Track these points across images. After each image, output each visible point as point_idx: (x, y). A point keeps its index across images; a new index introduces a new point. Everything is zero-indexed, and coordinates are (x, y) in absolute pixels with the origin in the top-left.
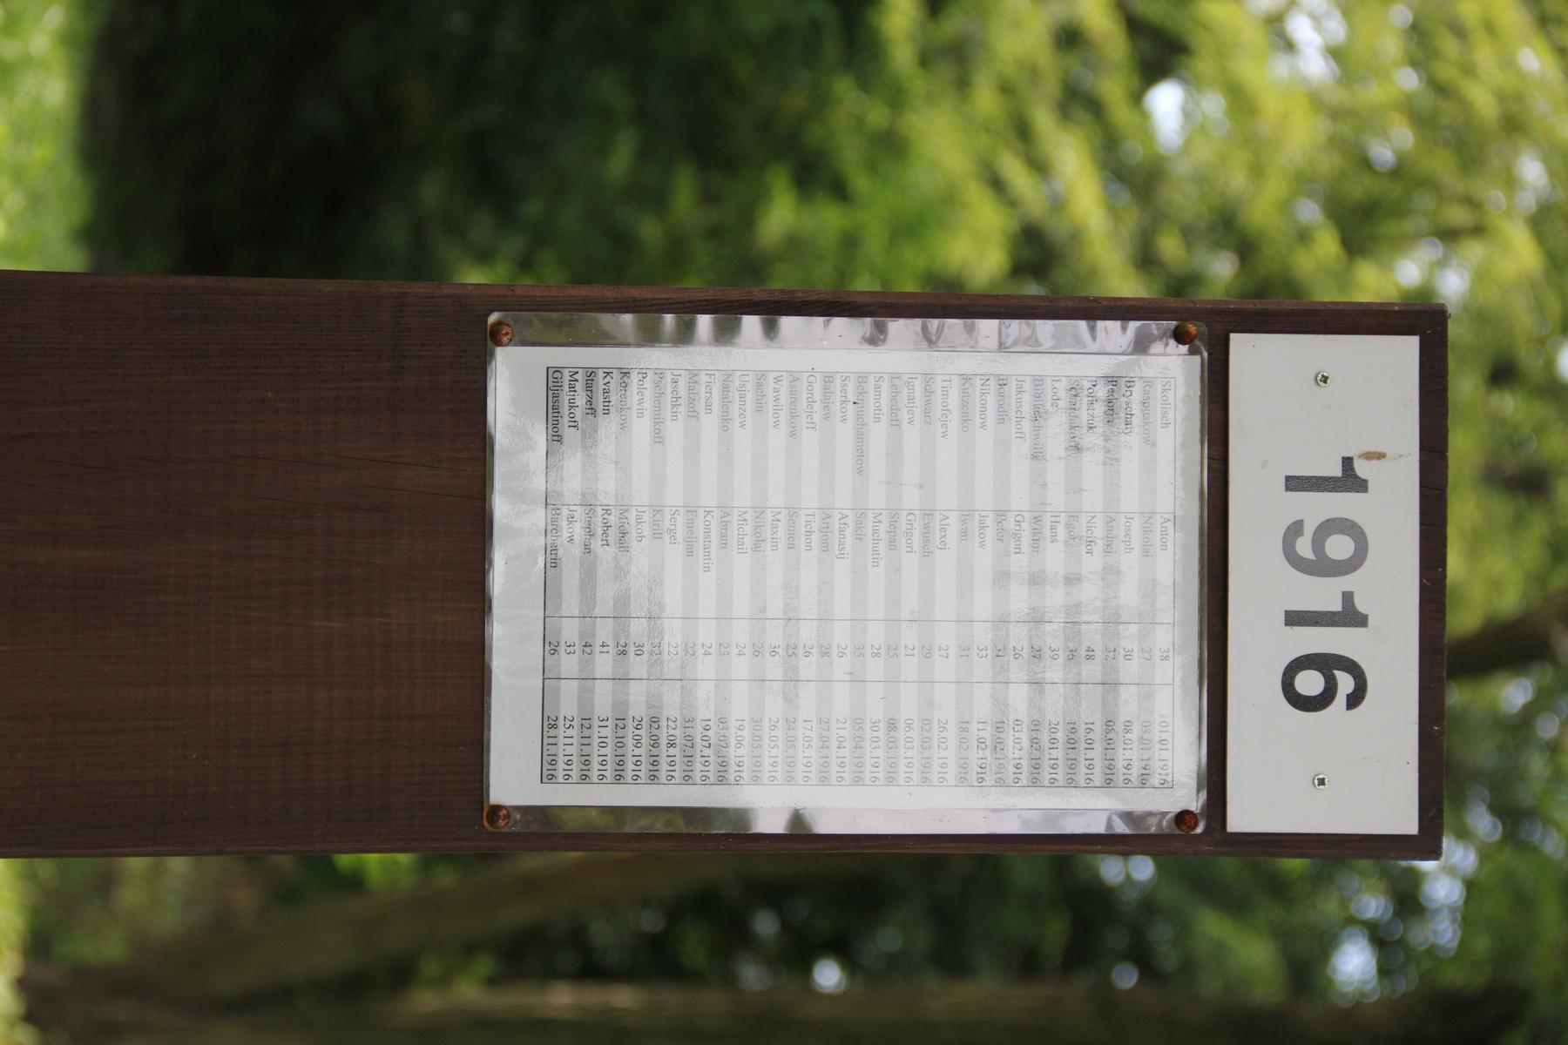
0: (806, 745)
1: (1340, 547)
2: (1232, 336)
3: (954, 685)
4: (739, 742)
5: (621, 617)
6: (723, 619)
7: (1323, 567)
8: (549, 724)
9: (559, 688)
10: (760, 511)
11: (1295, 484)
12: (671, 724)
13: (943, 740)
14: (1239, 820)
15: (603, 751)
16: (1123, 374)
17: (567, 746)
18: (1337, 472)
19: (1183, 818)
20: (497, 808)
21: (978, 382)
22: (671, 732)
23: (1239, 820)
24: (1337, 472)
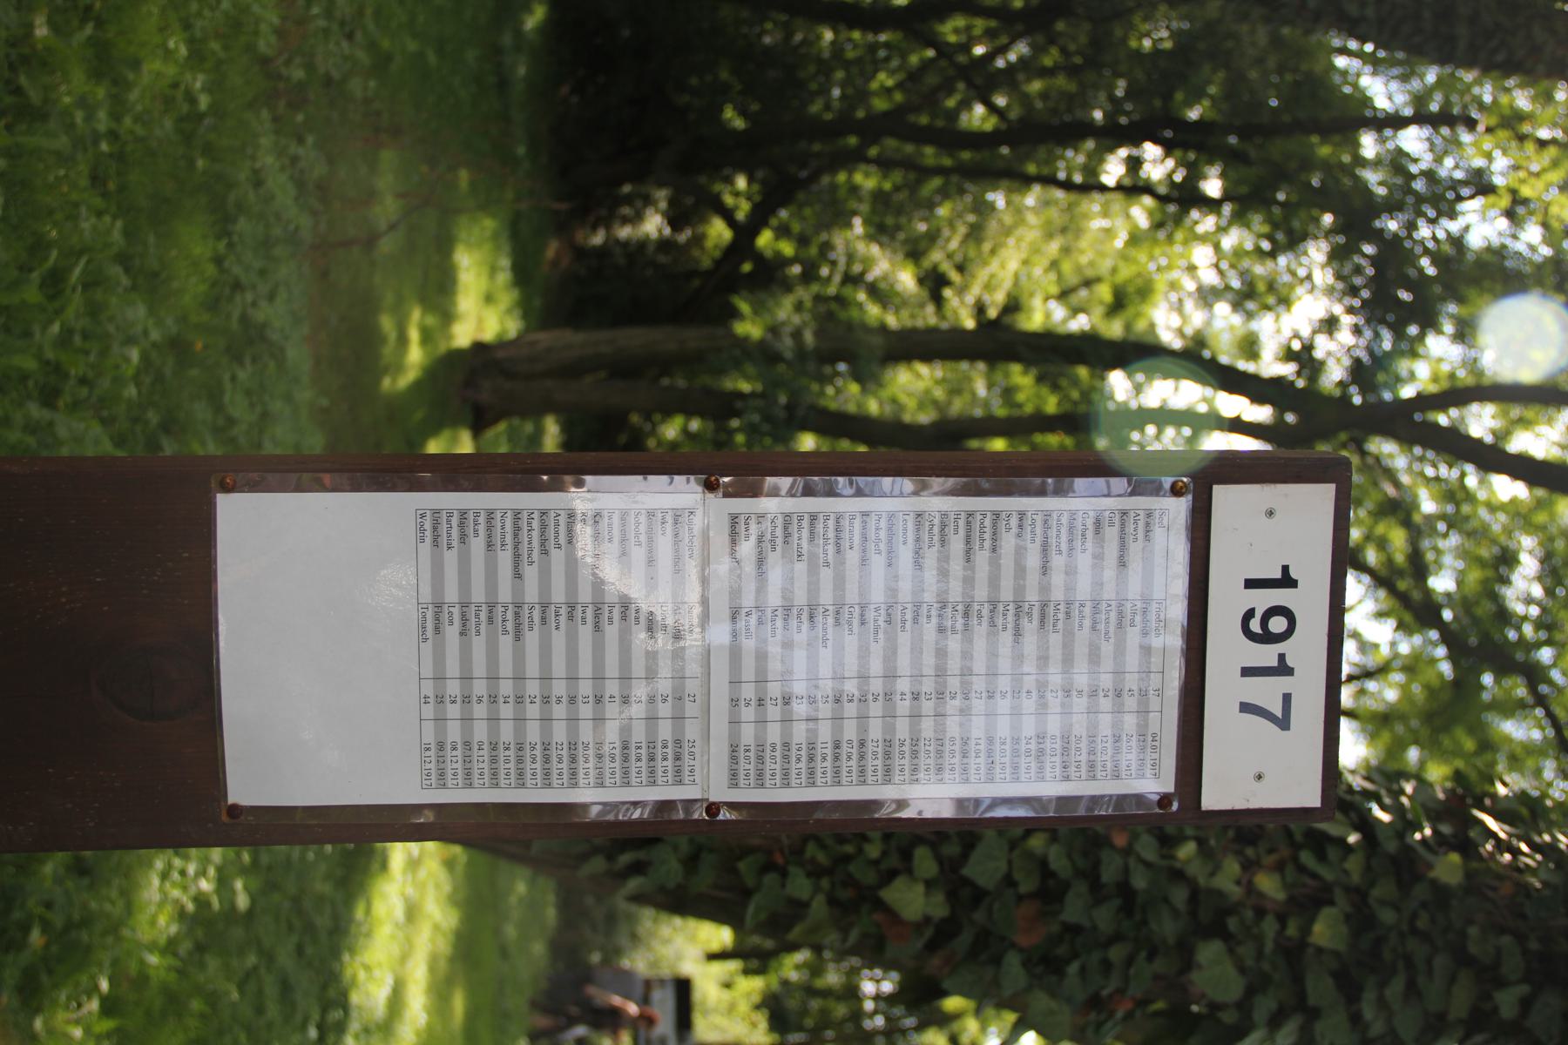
0: (874, 757)
1: (1278, 624)
2: (1215, 487)
3: (794, 719)
4: (799, 759)
5: (761, 680)
6: (572, 678)
7: (1267, 638)
8: (734, 749)
9: (894, 724)
10: (518, 606)
11: (1251, 584)
12: (560, 747)
13: (902, 753)
14: (1214, 797)
15: (507, 766)
16: (847, 510)
17: (747, 766)
18: (1278, 575)
19: (1165, 800)
20: (235, 810)
21: (874, 517)
22: (927, 748)
23: (1214, 797)
24: (1278, 575)
